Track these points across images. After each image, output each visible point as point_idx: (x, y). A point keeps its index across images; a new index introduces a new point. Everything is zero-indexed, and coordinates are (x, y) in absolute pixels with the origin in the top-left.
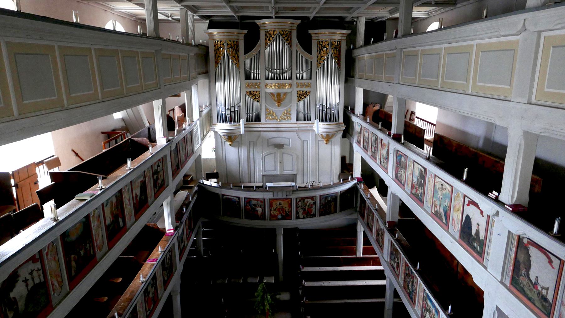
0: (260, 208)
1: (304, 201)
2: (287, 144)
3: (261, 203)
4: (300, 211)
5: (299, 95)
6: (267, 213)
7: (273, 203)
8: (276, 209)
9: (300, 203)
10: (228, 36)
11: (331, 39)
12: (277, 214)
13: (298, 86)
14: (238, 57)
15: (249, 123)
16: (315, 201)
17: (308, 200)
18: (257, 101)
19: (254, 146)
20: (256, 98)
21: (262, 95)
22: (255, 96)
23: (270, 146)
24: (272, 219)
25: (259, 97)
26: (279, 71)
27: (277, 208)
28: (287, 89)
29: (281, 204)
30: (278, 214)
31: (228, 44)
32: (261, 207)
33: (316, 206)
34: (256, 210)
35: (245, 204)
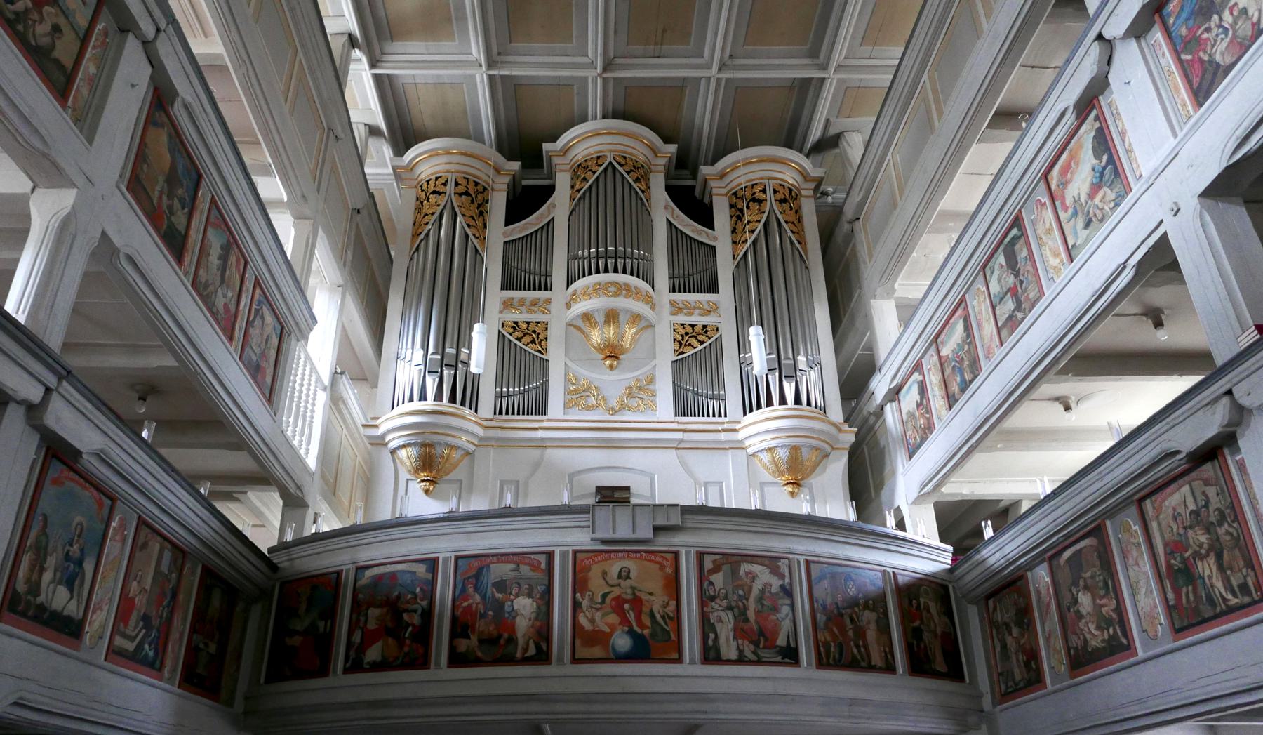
0: (530, 600)
1: (735, 572)
3: (532, 573)
4: (720, 620)
5: (682, 336)
6: (561, 628)
7: (589, 569)
8: (603, 602)
9: (718, 579)
11: (769, 179)
12: (608, 630)
13: (676, 309)
16: (787, 580)
17: (757, 569)
24: (583, 652)
25: (546, 338)
27: (608, 599)
29: (628, 577)
30: (613, 628)
31: (457, 184)
32: (530, 595)
33: (792, 606)
34: (507, 608)
35: (459, 587)
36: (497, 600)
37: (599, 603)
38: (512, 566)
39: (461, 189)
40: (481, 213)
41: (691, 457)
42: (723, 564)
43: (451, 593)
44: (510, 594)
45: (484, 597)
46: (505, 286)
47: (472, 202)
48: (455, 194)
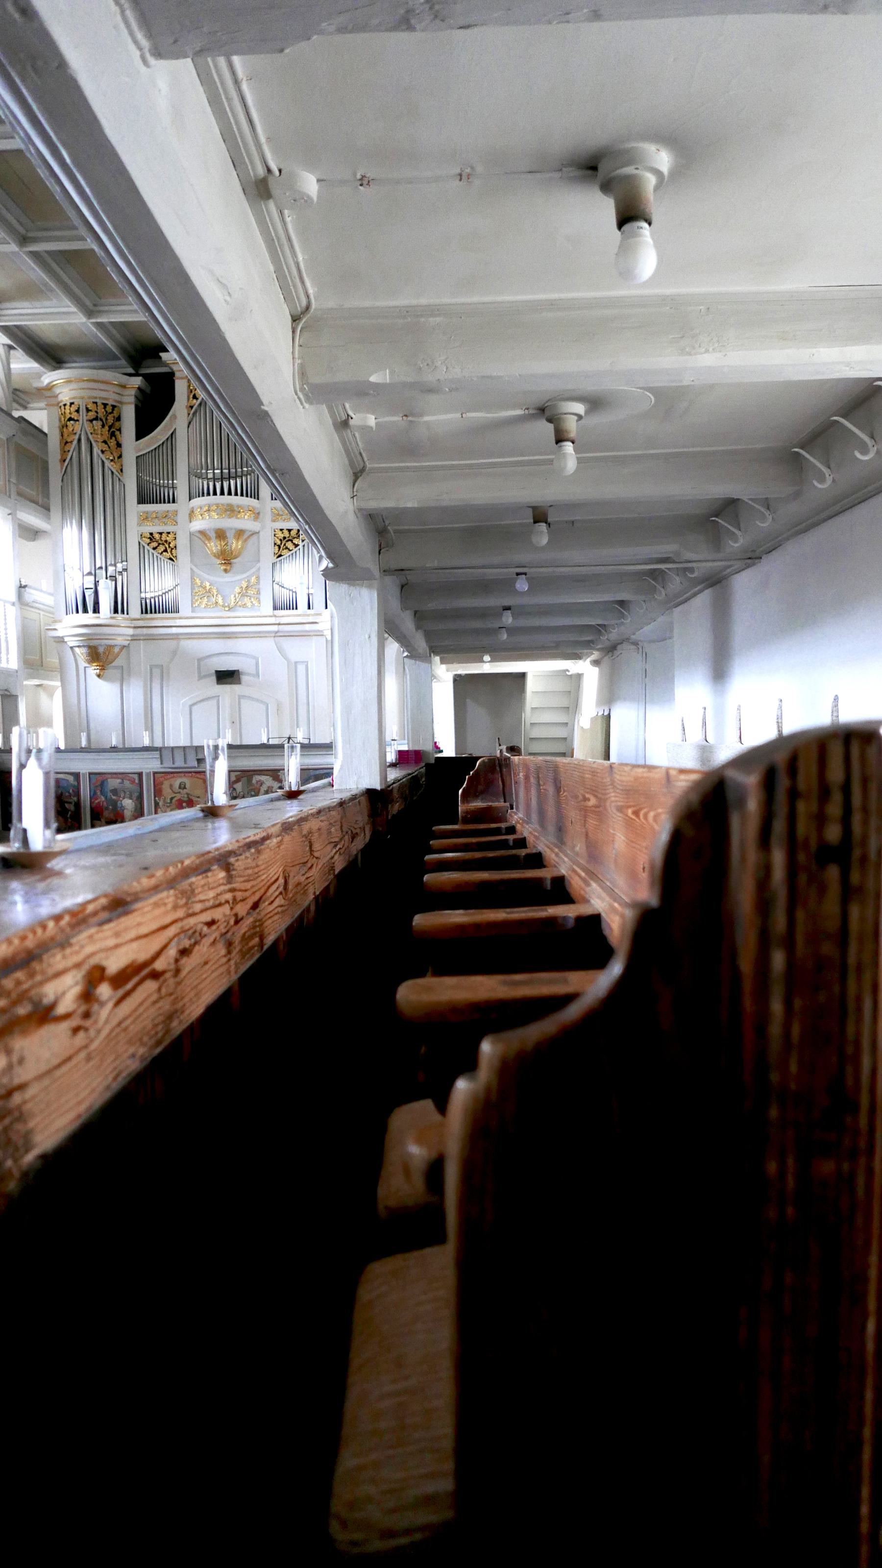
0: (131, 801)
1: (249, 781)
2: (252, 672)
5: (281, 540)
7: (162, 783)
8: (171, 802)
10: (90, 389)
14: (119, 445)
15: (149, 616)
17: (263, 778)
18: (171, 559)
19: (162, 680)
20: (166, 551)
21: (182, 543)
22: (163, 544)
23: (205, 676)
25: (175, 547)
26: (219, 471)
27: (174, 801)
28: (245, 523)
29: (185, 788)
31: (88, 410)
32: (131, 798)
34: (119, 805)
35: (93, 791)
36: (113, 800)
37: (169, 803)
38: (119, 781)
39: (92, 415)
40: (113, 435)
41: (287, 643)
42: (242, 777)
43: (88, 792)
44: (120, 797)
45: (106, 798)
46: (142, 500)
47: (103, 426)
48: (87, 420)
